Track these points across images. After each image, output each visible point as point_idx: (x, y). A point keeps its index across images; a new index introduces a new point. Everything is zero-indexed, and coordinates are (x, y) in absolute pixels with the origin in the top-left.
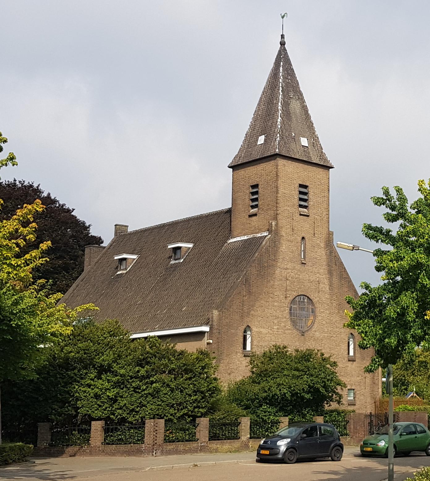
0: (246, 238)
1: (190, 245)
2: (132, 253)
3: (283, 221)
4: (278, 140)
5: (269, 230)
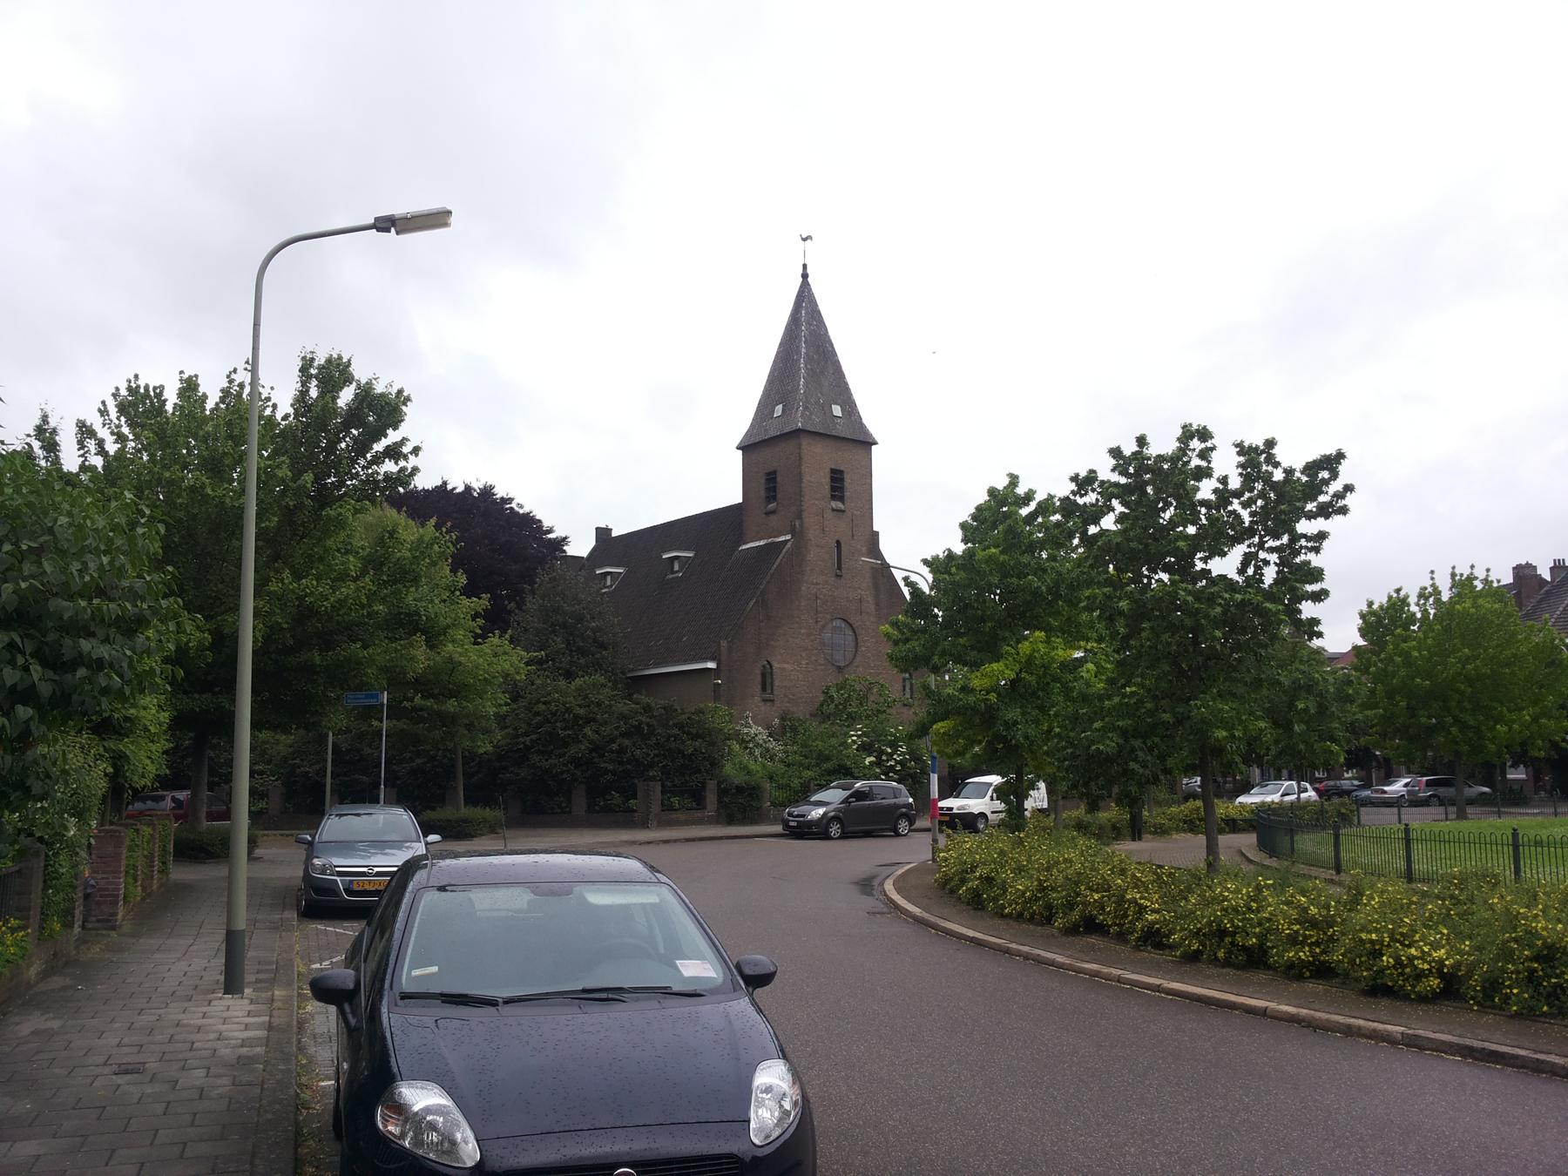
1: (691, 555)
3: (810, 520)
4: (807, 435)
5: (793, 532)
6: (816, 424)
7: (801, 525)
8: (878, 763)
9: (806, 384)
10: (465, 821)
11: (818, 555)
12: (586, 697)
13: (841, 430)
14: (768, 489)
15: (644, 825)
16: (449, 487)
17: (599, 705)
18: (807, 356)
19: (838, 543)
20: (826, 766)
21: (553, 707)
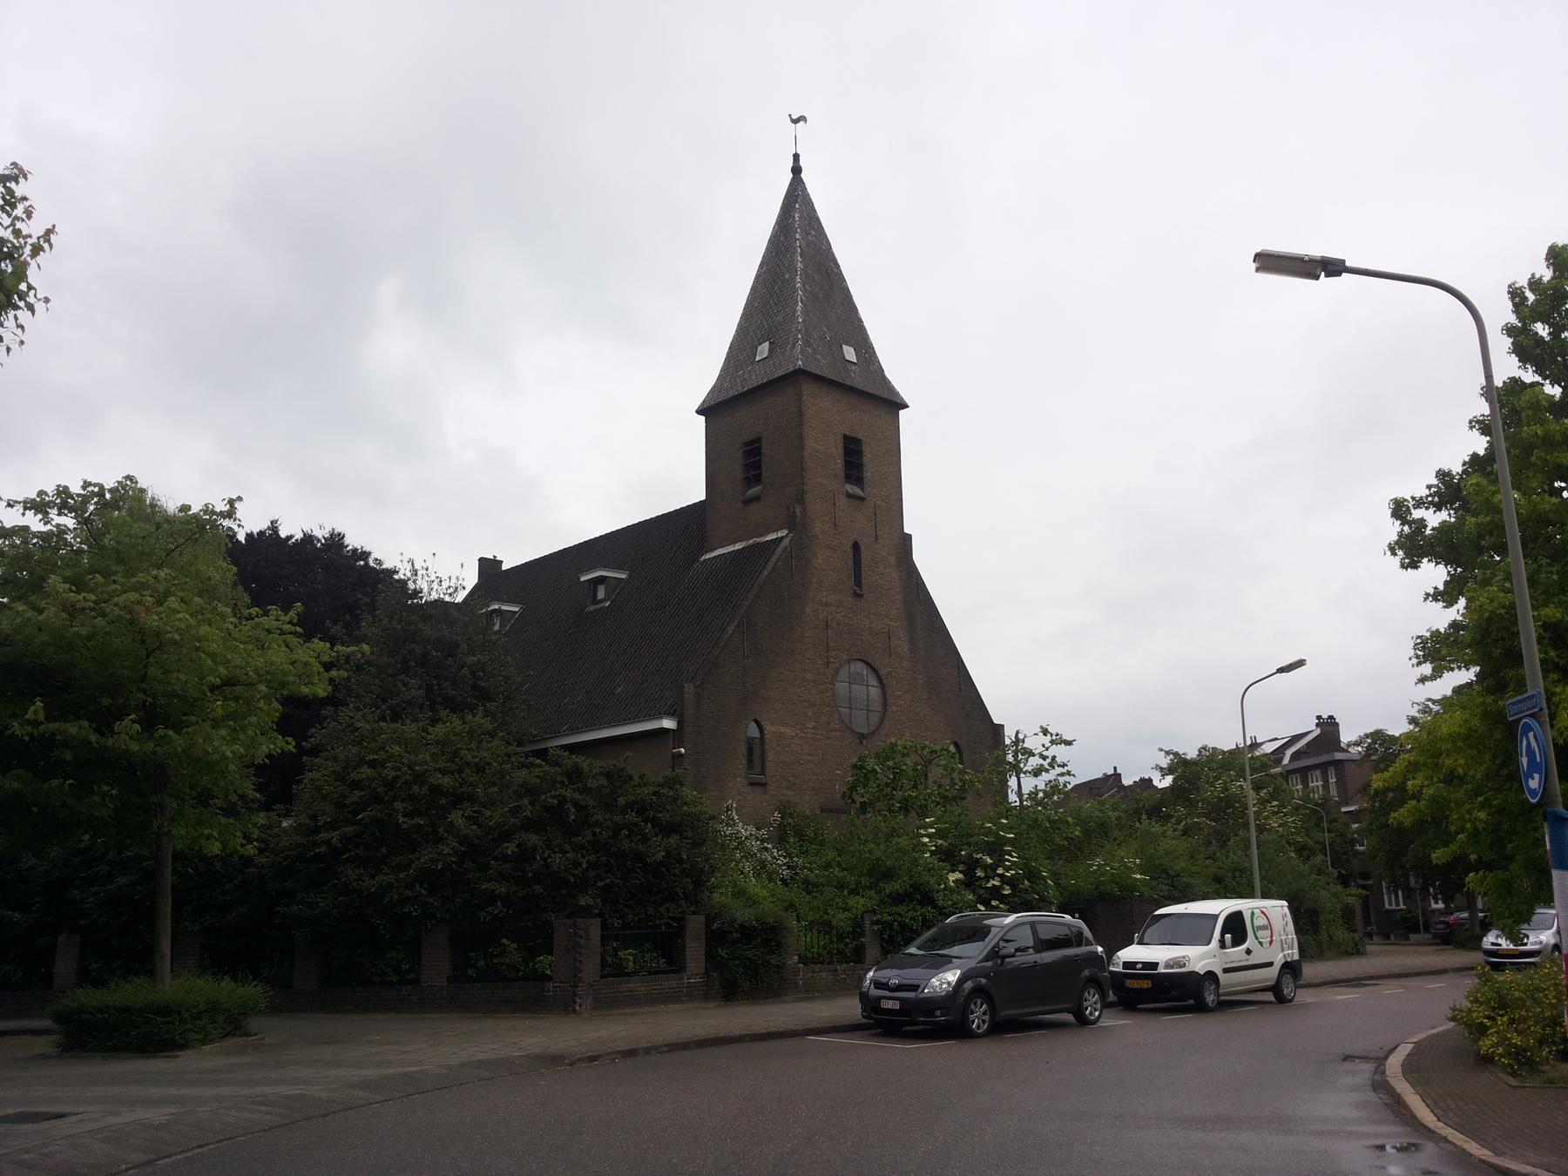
0: (738, 546)
2: (512, 601)
6: (822, 366)
7: (804, 512)
8: (970, 883)
9: (806, 312)
10: (164, 1011)
11: (828, 562)
12: (456, 753)
13: (858, 381)
14: (747, 467)
15: (565, 1006)
16: (283, 534)
17: (480, 768)
18: (799, 275)
19: (856, 546)
20: (889, 888)
21: (389, 773)
